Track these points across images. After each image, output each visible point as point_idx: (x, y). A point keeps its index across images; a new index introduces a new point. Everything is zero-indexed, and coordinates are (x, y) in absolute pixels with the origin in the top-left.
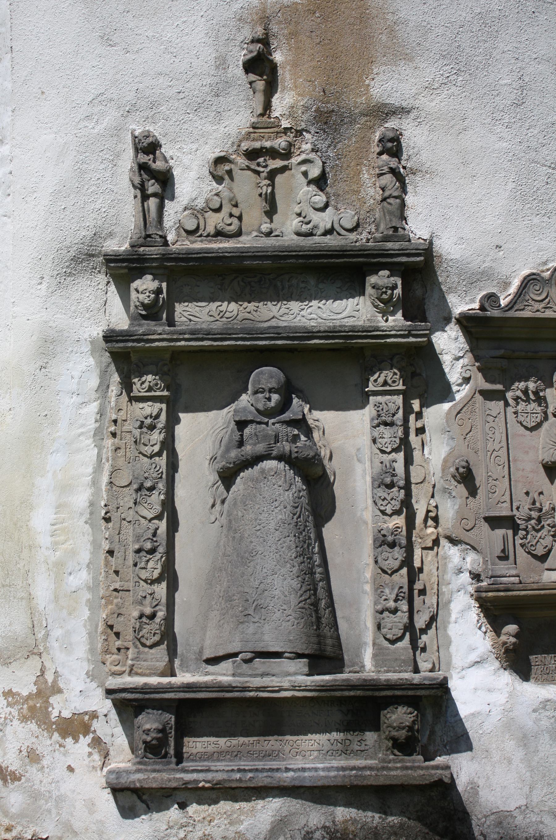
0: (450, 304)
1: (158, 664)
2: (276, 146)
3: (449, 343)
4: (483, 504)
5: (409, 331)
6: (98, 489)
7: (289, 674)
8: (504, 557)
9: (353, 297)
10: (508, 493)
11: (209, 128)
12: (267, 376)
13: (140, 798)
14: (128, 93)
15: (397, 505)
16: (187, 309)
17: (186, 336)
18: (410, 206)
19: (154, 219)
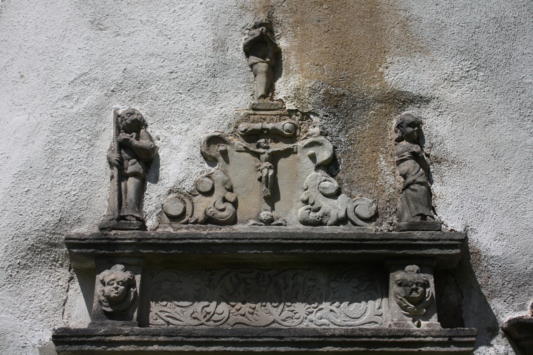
0: (494, 311)
5: (450, 338)
9: (374, 299)
11: (203, 107)
14: (115, 73)
16: (165, 309)
17: (161, 338)
18: (438, 195)
19: (131, 200)
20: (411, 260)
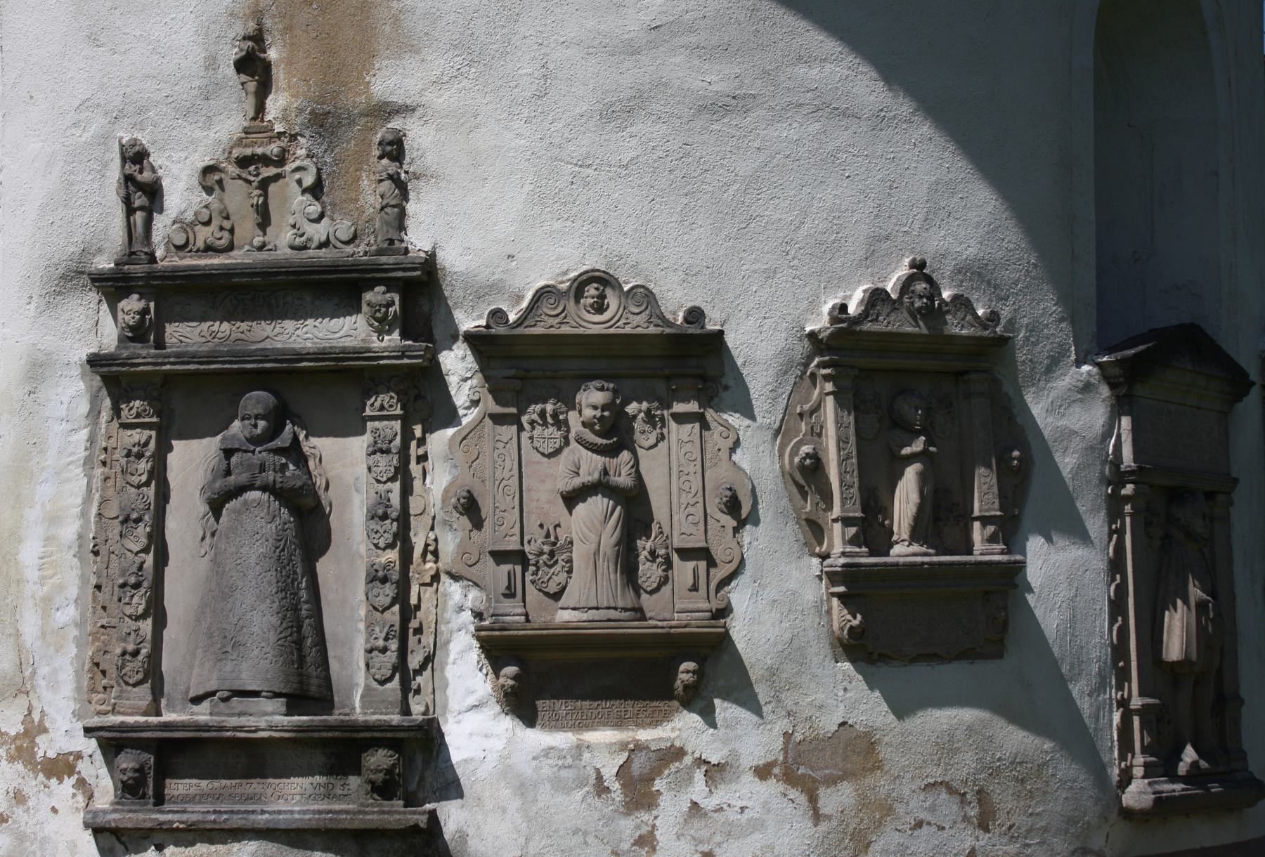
1: (141, 703)
2: (268, 153)
3: (456, 363)
4: (488, 537)
6: (88, 521)
7: (266, 714)
8: (509, 594)
10: (518, 525)
11: (199, 134)
12: (257, 400)
13: (118, 839)
17: (172, 360)
20: (379, 282)
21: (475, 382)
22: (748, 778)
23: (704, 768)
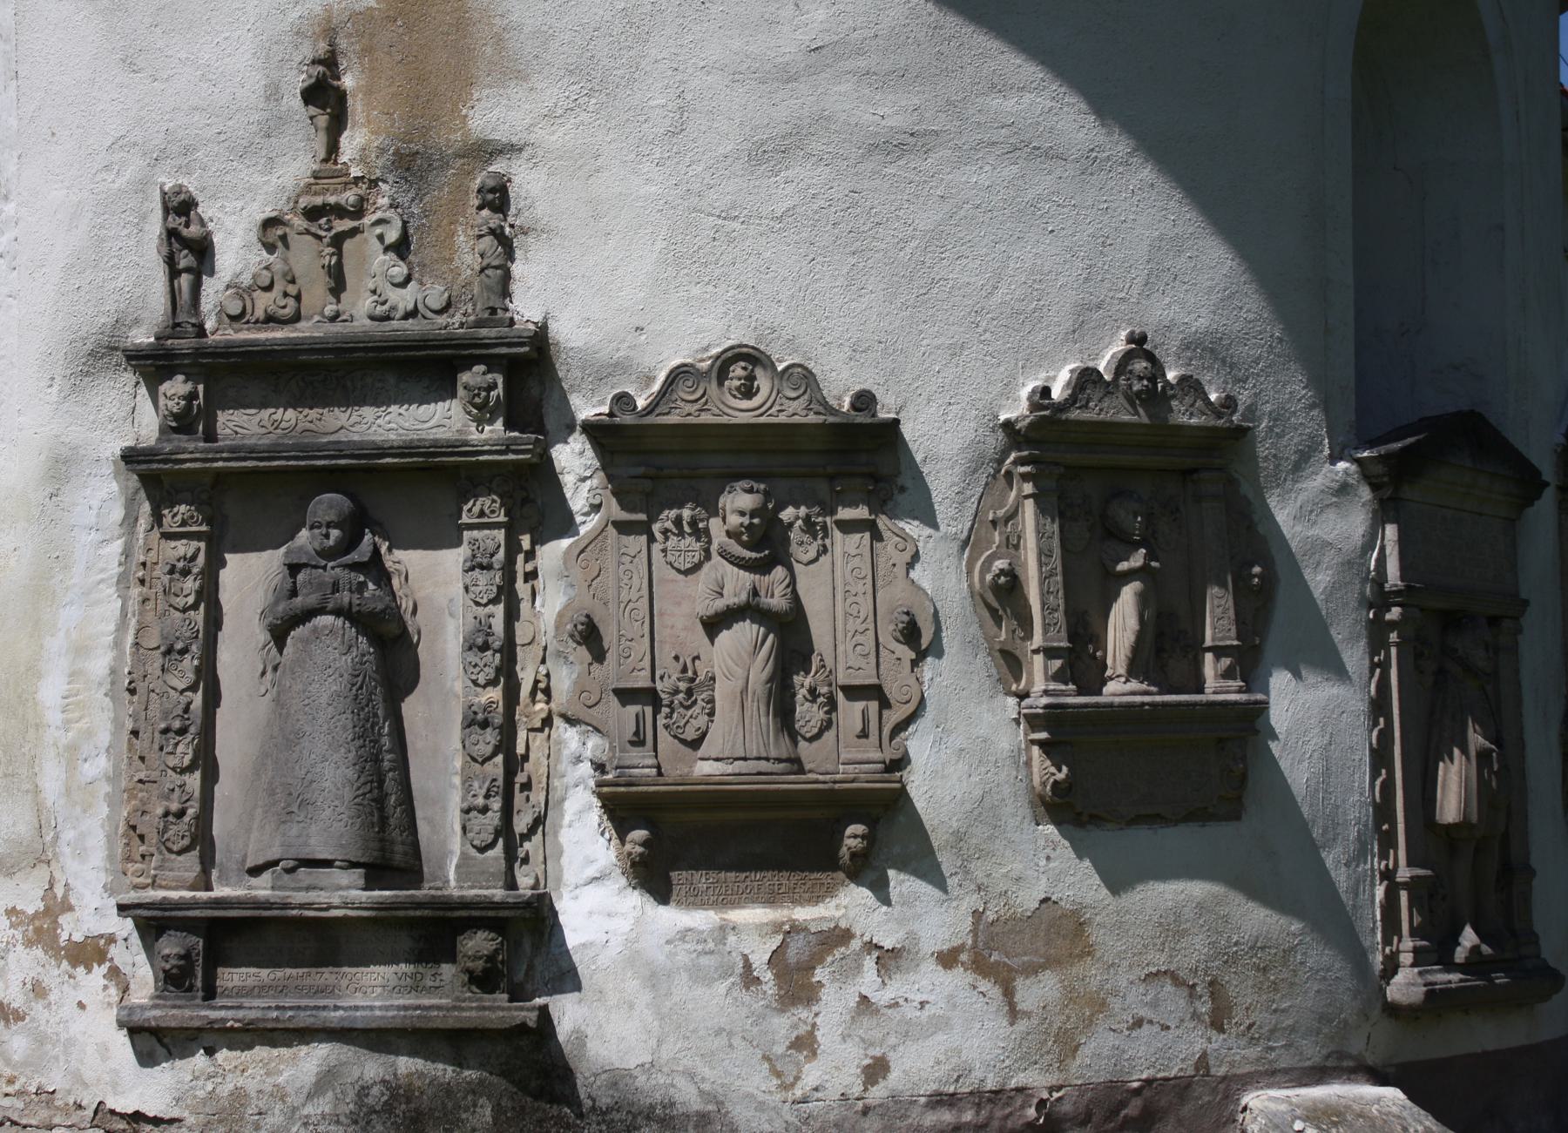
2: (343, 202)
3: (573, 460)
4: (612, 672)
6: (121, 653)
7: (340, 888)
8: (638, 742)
9: (444, 400)
10: (648, 658)
11: (258, 179)
12: (329, 504)
13: (160, 1041)
15: (490, 672)
20: (479, 360)
21: (595, 482)
22: (930, 967)
23: (875, 954)
